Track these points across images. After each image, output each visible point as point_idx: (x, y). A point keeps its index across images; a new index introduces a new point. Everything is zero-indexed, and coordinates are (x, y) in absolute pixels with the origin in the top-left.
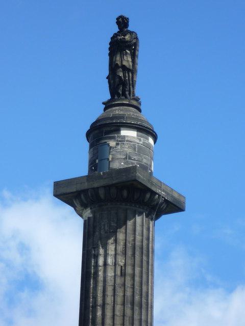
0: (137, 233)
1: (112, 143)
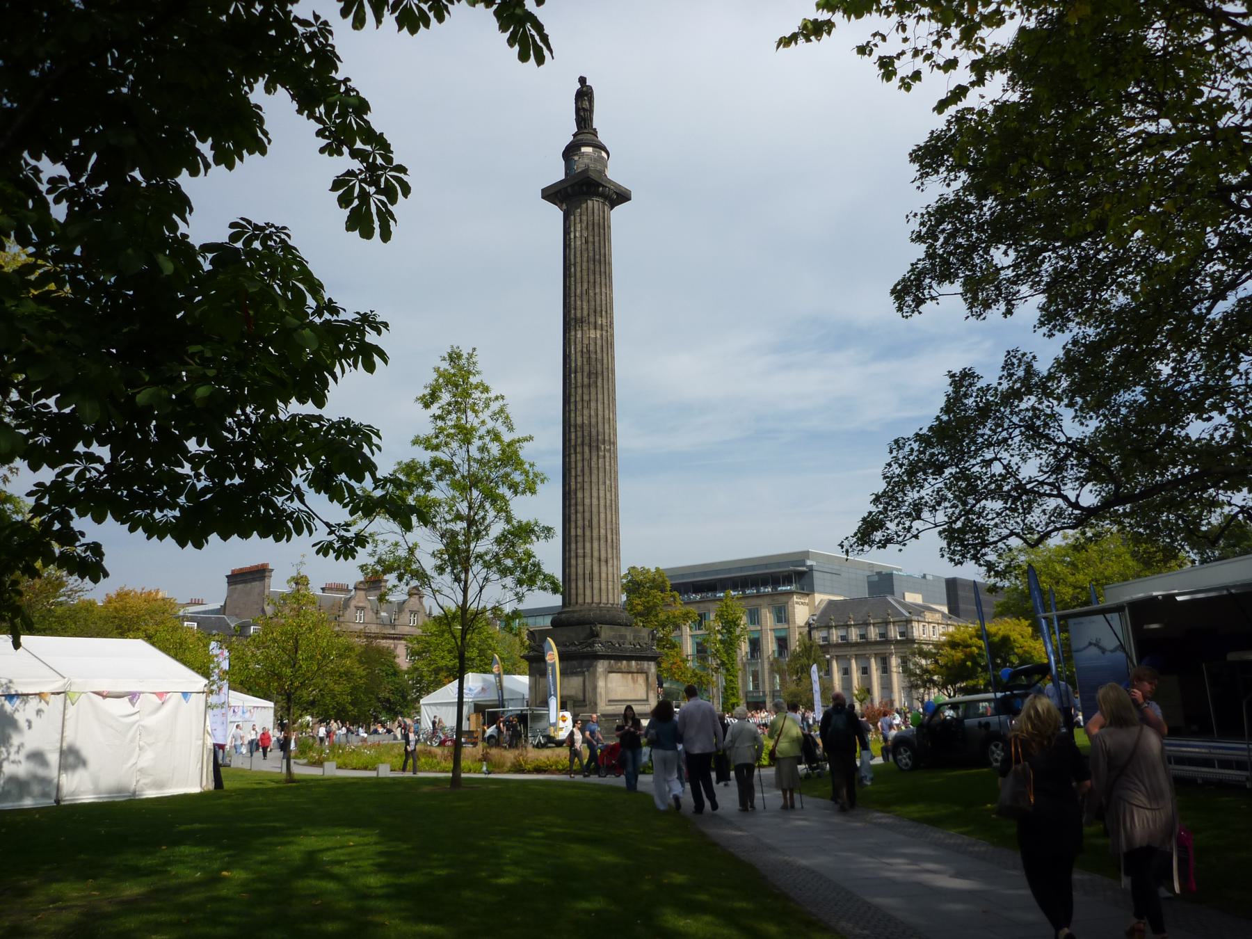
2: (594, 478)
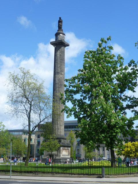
1: (59, 36)
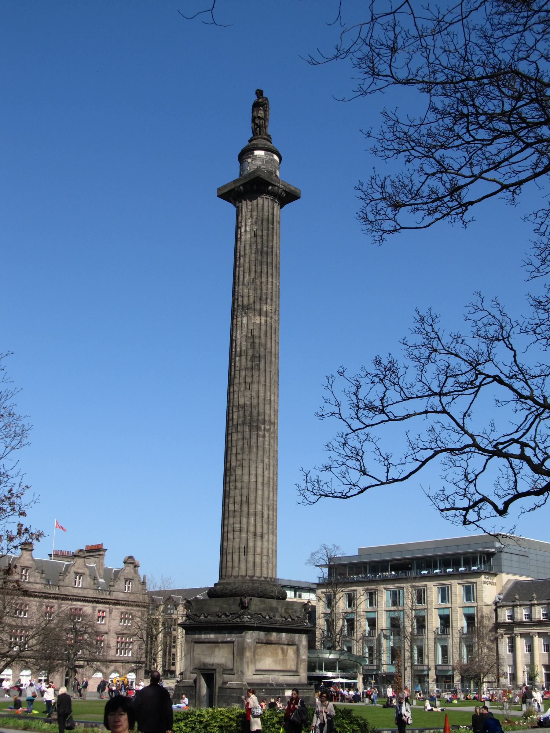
0: (265, 211)
1: (249, 160)
2: (253, 457)
